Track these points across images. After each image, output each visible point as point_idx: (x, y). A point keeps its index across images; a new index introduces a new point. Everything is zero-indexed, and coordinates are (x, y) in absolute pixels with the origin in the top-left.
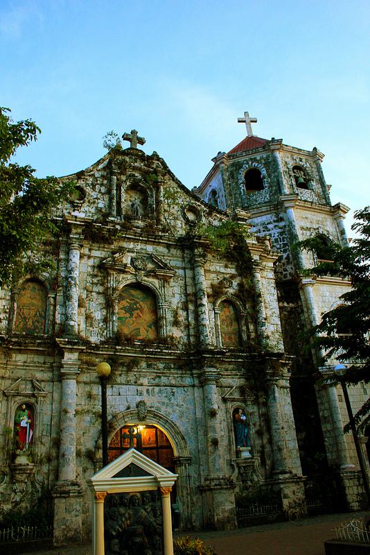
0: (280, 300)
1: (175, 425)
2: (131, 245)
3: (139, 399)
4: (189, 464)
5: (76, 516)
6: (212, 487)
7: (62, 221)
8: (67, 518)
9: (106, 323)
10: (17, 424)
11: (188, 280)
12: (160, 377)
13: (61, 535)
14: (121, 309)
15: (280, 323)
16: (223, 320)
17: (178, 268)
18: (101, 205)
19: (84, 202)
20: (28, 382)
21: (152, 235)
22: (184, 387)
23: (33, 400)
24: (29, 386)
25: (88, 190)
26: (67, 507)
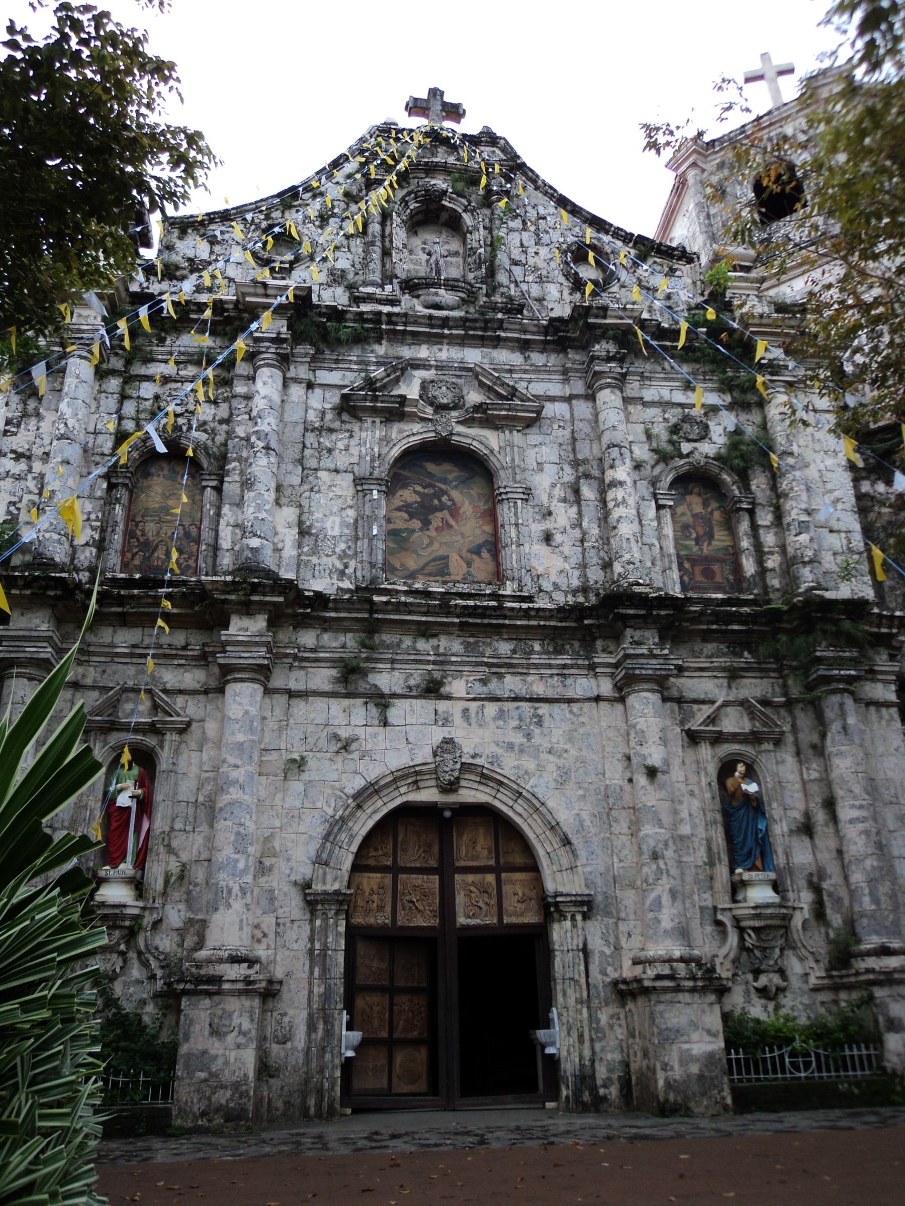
0: (857, 474)
2: (423, 352)
3: (438, 734)
4: (586, 917)
5: (239, 1046)
6: (647, 983)
8: (213, 1052)
12: (501, 676)
14: (399, 509)
15: (857, 527)
16: (685, 527)
17: (552, 399)
18: (343, 263)
22: (570, 701)
23: (151, 741)
24: (145, 704)
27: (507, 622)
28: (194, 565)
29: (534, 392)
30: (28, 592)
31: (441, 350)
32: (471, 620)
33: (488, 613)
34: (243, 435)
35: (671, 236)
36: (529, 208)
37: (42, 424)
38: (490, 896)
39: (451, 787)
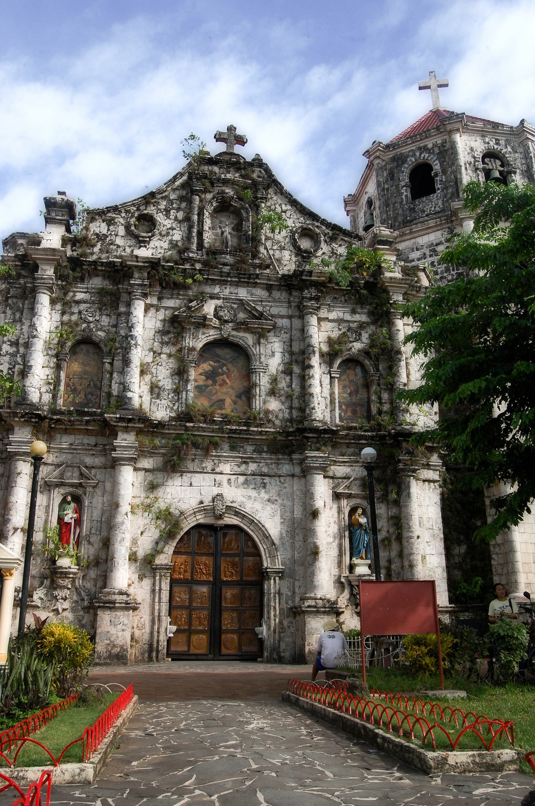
1: (263, 526)
2: (217, 290)
3: (216, 491)
4: (280, 578)
5: (123, 630)
7: (121, 263)
8: (111, 632)
9: (178, 393)
10: (60, 520)
11: (294, 332)
13: (105, 650)
17: (282, 317)
19: (153, 236)
20: (75, 469)
21: (244, 274)
22: (280, 476)
24: (76, 474)
25: (160, 218)
26: (113, 619)
27: (251, 437)
28: (98, 402)
29: (273, 313)
30: (23, 420)
31: (226, 288)
32: (234, 436)
33: (242, 432)
34: (124, 335)
35: (366, 190)
36: (277, 206)
37: (23, 327)
38: (237, 568)
39: (220, 517)
